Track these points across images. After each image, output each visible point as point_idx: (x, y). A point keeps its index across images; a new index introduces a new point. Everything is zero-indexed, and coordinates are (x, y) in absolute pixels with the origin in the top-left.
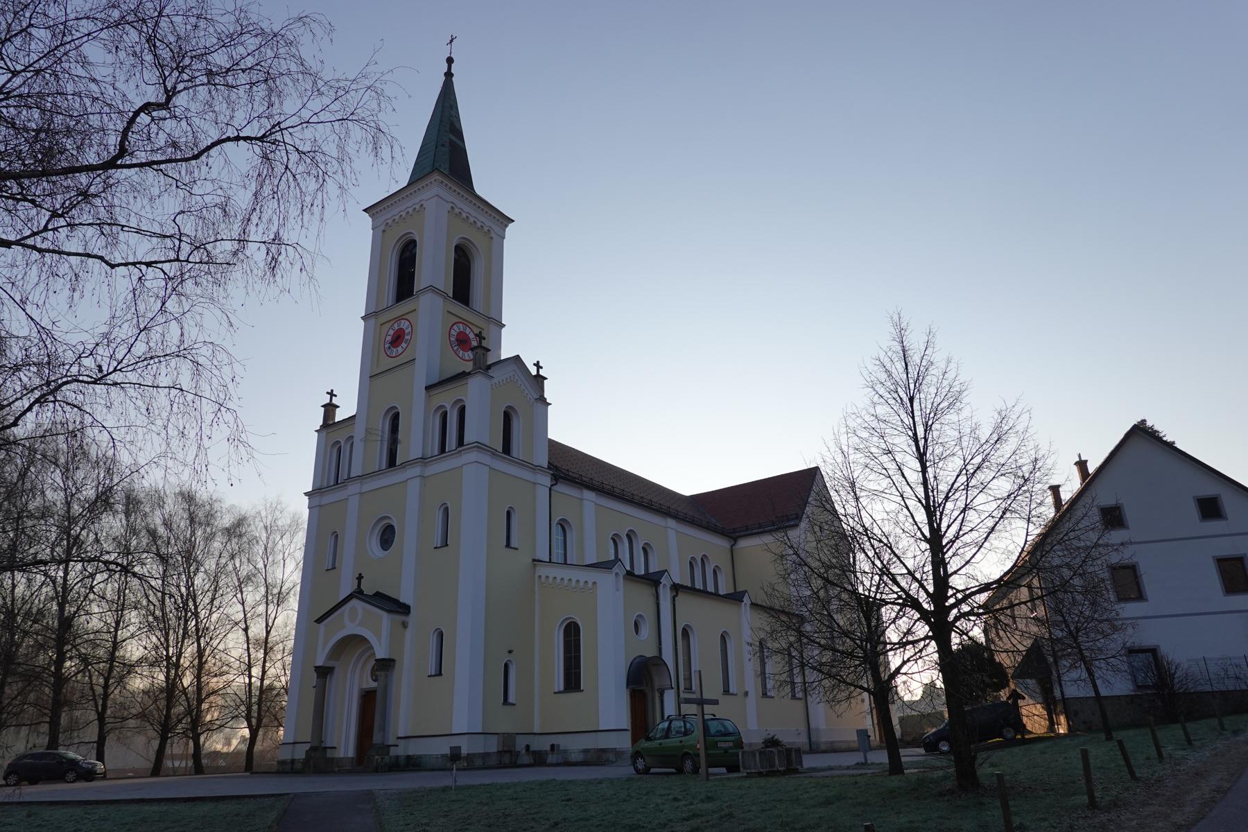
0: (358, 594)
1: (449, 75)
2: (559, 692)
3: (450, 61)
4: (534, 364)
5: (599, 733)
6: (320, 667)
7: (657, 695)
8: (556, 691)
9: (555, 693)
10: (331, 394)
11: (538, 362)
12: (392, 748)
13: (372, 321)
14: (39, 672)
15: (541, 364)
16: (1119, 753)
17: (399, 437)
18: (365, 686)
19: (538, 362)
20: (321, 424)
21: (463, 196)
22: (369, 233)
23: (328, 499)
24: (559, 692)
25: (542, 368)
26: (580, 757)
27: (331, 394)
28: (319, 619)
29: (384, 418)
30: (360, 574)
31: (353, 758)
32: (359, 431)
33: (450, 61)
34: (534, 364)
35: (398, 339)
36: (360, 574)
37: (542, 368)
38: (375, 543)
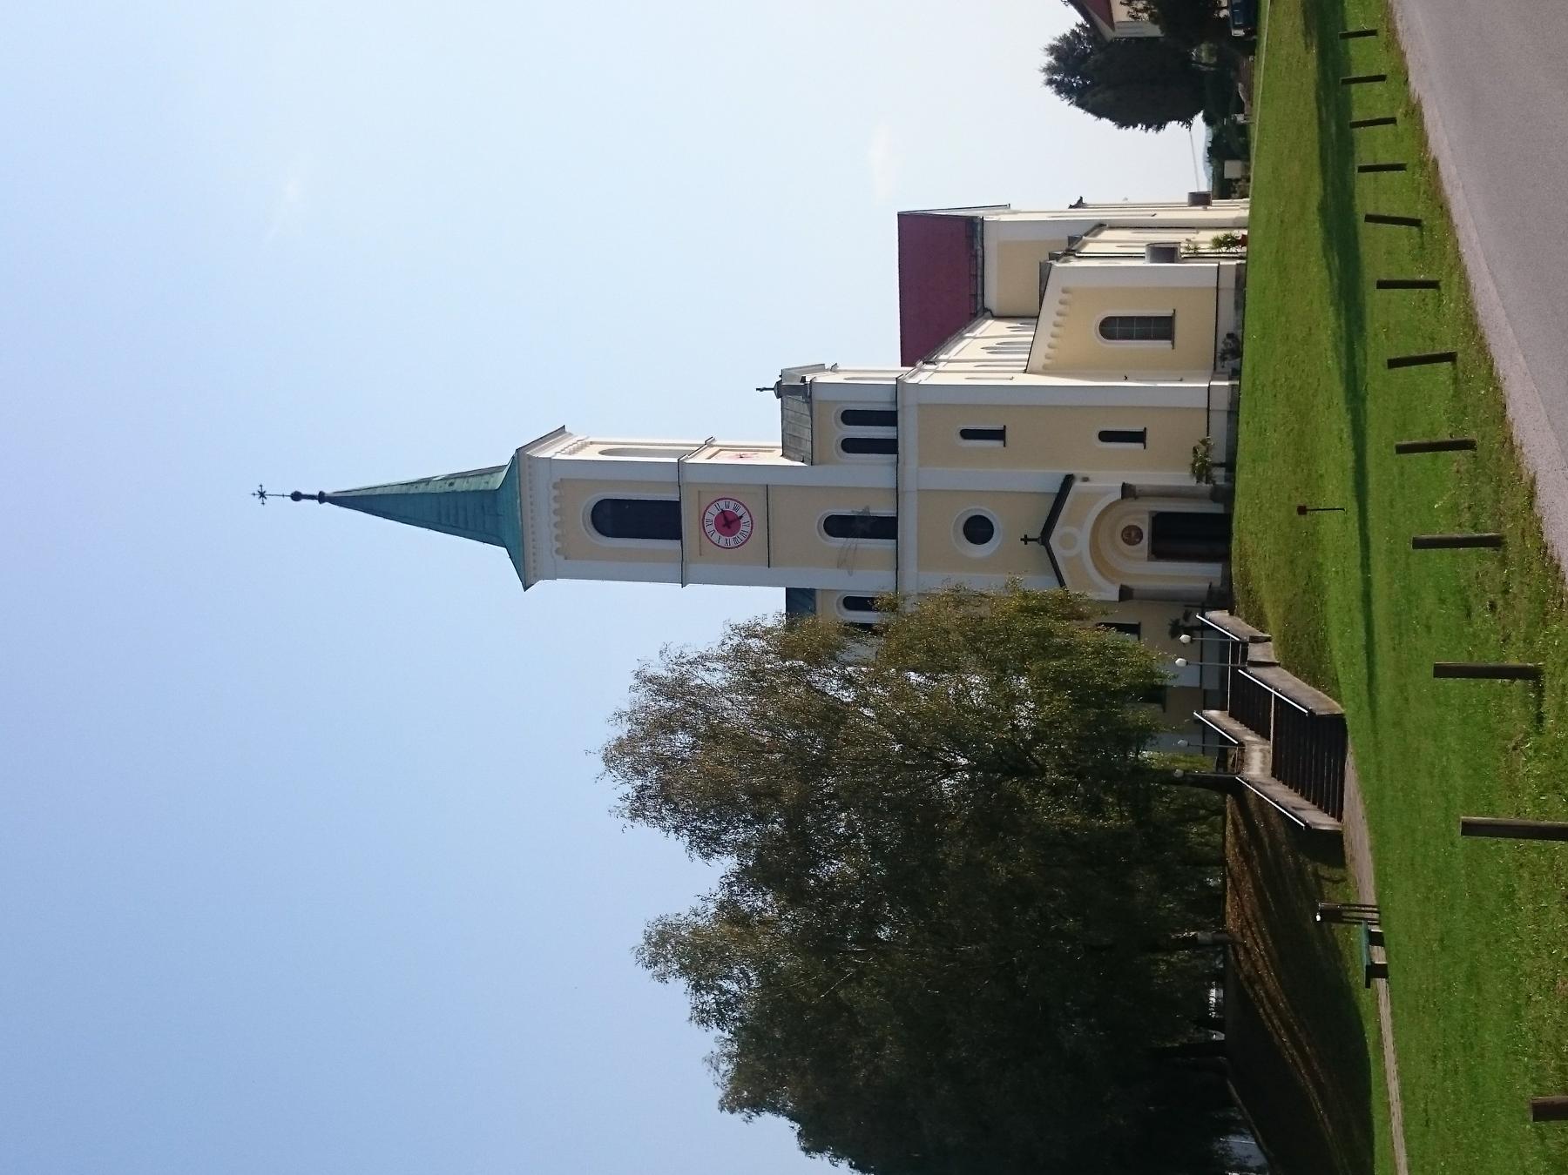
1: (322, 498)
2: (1173, 344)
3: (297, 496)
22: (562, 583)
24: (1173, 344)
33: (297, 496)
35: (728, 523)
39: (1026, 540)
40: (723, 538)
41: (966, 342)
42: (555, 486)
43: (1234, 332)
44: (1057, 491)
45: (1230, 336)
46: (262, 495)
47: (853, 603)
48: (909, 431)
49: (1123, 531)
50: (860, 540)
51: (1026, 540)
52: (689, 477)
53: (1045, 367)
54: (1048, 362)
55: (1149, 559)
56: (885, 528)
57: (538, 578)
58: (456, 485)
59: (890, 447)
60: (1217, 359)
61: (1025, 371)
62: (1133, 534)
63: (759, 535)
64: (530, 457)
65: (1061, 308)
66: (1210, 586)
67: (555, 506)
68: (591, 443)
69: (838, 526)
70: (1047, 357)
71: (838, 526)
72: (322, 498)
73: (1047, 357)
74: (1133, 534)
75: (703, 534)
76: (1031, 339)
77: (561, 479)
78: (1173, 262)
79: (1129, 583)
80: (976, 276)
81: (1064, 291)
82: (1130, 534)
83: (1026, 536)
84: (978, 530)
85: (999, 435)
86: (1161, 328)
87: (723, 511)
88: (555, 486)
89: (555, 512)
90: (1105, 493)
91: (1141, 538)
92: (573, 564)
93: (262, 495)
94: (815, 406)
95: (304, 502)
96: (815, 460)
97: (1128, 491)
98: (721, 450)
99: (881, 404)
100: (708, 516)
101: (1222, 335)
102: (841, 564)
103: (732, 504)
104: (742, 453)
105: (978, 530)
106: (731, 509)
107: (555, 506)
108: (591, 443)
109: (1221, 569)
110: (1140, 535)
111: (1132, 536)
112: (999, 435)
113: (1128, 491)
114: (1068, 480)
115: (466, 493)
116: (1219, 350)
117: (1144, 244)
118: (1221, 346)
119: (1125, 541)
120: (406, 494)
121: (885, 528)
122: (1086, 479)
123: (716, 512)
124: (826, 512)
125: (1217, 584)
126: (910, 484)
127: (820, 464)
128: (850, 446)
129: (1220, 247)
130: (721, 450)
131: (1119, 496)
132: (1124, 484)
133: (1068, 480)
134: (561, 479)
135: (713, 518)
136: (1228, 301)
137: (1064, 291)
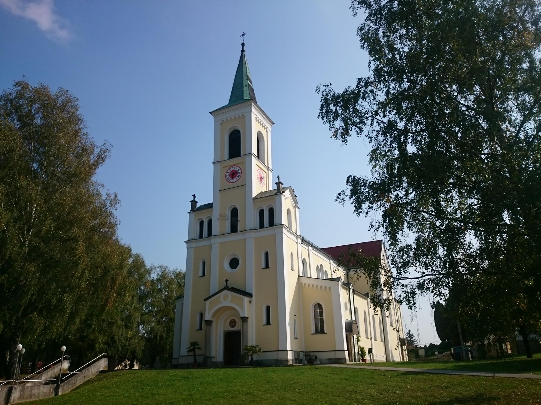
0: (226, 288)
1: (243, 51)
2: (314, 334)
3: (243, 44)
4: (193, 196)
5: (336, 352)
6: (208, 321)
7: (352, 336)
8: (313, 333)
9: (312, 334)
10: (194, 196)
11: (194, 195)
12: (213, 358)
13: (218, 165)
14: (148, 310)
15: (195, 196)
16: (444, 375)
17: (239, 219)
18: (226, 330)
19: (194, 195)
20: (190, 210)
21: (230, 111)
22: (213, 124)
23: (194, 245)
24: (314, 334)
25: (196, 197)
26: (328, 362)
27: (194, 196)
28: (205, 299)
29: (229, 210)
30: (227, 279)
31: (222, 362)
32: (215, 214)
33: (243, 44)
34: (193, 196)
35: (234, 174)
36: (227, 279)
37: (196, 197)
38: (226, 265)
39: (227, 281)
40: (229, 174)
41: (328, 261)
42: (243, 115)
43: (318, 359)
44: (247, 291)
45: (316, 357)
46: (243, 35)
47: (210, 222)
48: (267, 232)
49: (234, 319)
50: (230, 221)
51: (227, 281)
52: (247, 158)
53: (301, 284)
54: (303, 285)
55: (224, 331)
56: (234, 229)
57: (214, 116)
58: (246, 87)
59: (262, 226)
60: (306, 353)
61: (299, 276)
62: (233, 324)
63: (231, 185)
64: (251, 104)
65: (323, 287)
66: (212, 357)
67: (237, 116)
68: (267, 131)
69: (234, 212)
70: (305, 284)
71: (234, 212)
72: (243, 51)
73: (305, 284)
74: (233, 324)
75: (230, 167)
76: (309, 276)
77: (245, 116)
78: (346, 331)
79: (214, 325)
80: (354, 267)
81: (330, 288)
82: (233, 322)
83: (228, 280)
84: (234, 263)
85: (267, 266)
86: (320, 330)
87: (237, 172)
88: (243, 115)
89: (235, 117)
90: (242, 307)
91: (232, 327)
92: (220, 125)
93: (243, 35)
94: (274, 196)
95: (242, 47)
96: (254, 200)
97: (245, 319)
98: (266, 173)
99: (276, 221)
100: (236, 167)
101: (316, 354)
102: (221, 215)
103: (240, 174)
104: (265, 179)
105: (234, 263)
106: (238, 174)
107: (237, 116)
108: (267, 131)
109: (221, 361)
110: (233, 326)
111: (233, 323)
112: (267, 266)
113: (245, 319)
114: (250, 295)
115: (243, 90)
116: (310, 353)
117: (354, 319)
118: (312, 354)
119: (231, 321)
120: (243, 73)
121: (234, 229)
122: (250, 302)
123: (237, 170)
124: (237, 206)
125: (214, 360)
126: (247, 235)
127: (254, 202)
128: (261, 212)
129: (361, 350)
130: (266, 173)
131: (242, 316)
132: (247, 318)
133: (250, 295)
134: (245, 116)
135: (235, 169)
136: (331, 355)
137: (330, 288)
